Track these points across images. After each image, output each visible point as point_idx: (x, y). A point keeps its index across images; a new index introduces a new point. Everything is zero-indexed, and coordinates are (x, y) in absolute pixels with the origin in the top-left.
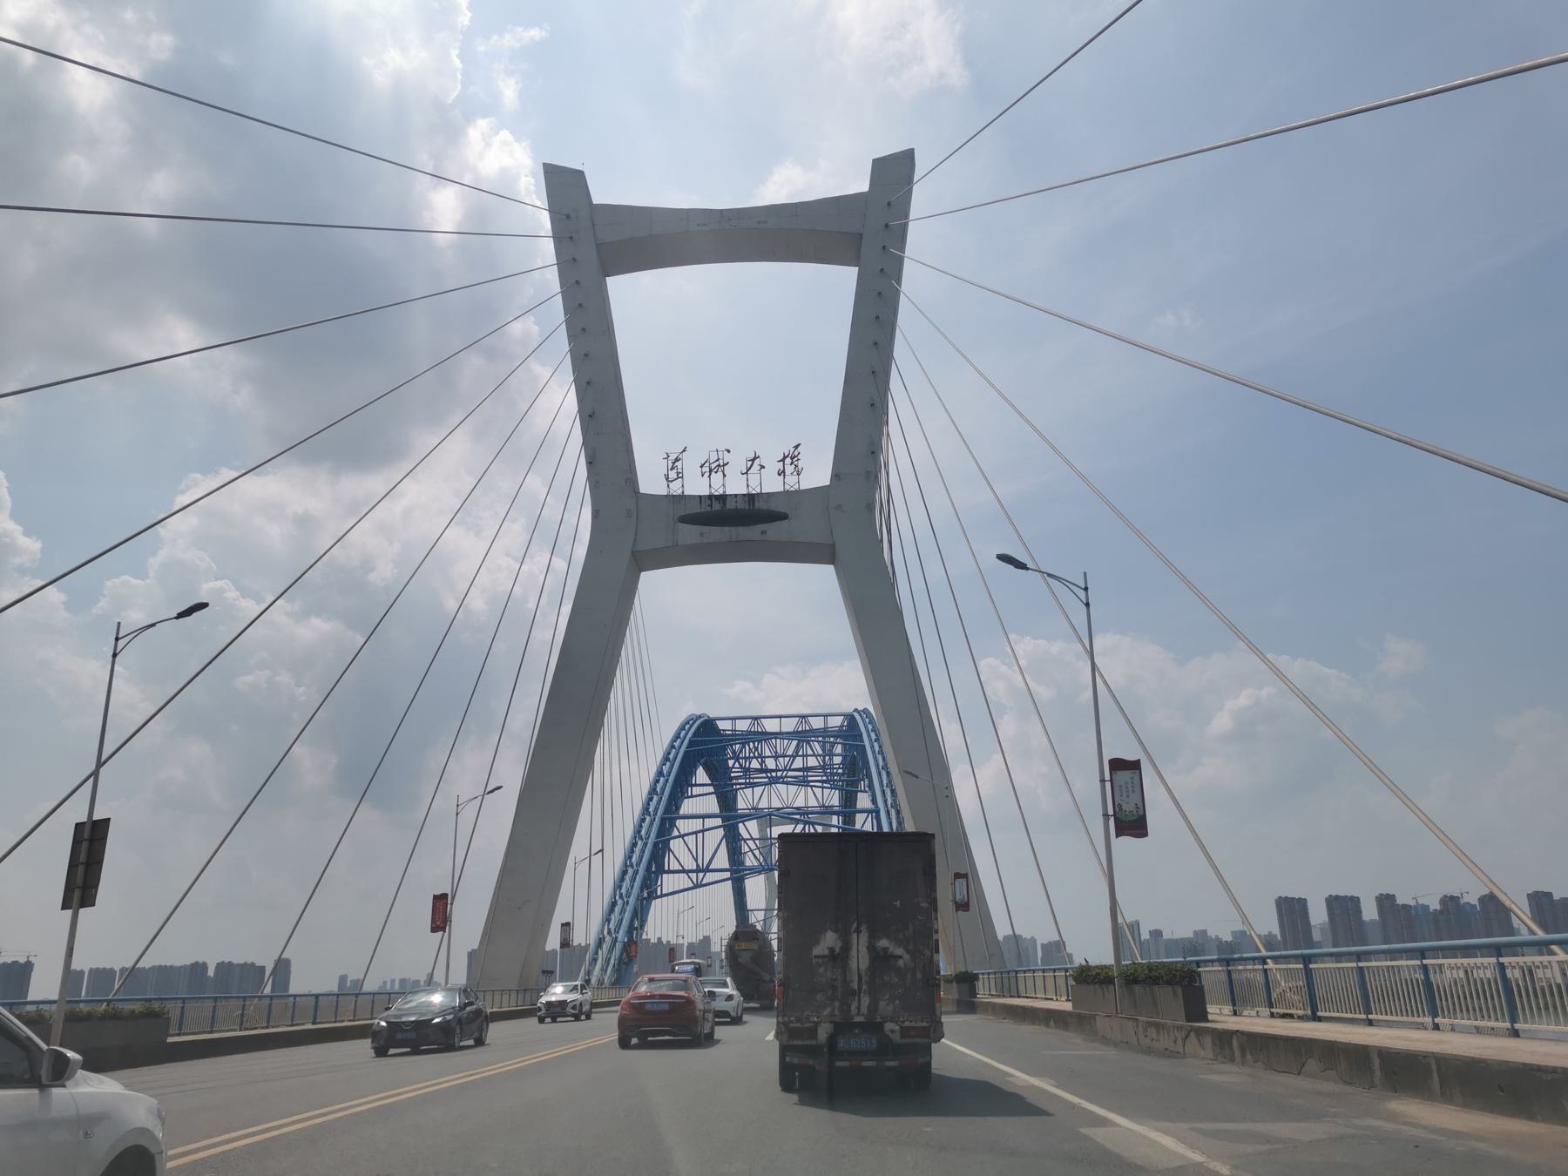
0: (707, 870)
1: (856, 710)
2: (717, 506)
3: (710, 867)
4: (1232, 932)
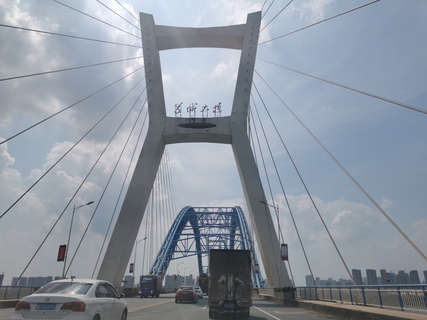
0: (188, 251)
1: (236, 206)
2: (192, 122)
3: (189, 251)
4: (339, 279)
